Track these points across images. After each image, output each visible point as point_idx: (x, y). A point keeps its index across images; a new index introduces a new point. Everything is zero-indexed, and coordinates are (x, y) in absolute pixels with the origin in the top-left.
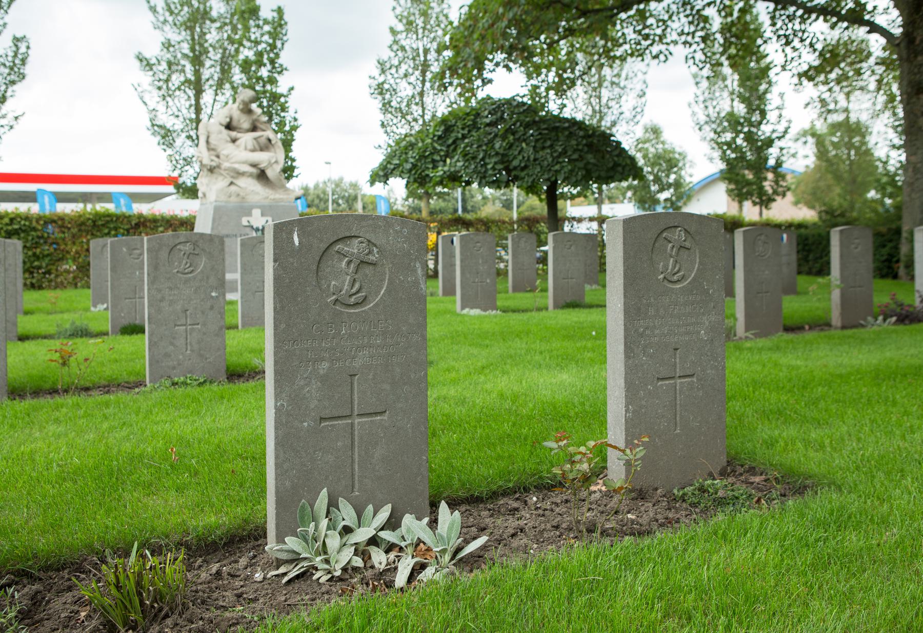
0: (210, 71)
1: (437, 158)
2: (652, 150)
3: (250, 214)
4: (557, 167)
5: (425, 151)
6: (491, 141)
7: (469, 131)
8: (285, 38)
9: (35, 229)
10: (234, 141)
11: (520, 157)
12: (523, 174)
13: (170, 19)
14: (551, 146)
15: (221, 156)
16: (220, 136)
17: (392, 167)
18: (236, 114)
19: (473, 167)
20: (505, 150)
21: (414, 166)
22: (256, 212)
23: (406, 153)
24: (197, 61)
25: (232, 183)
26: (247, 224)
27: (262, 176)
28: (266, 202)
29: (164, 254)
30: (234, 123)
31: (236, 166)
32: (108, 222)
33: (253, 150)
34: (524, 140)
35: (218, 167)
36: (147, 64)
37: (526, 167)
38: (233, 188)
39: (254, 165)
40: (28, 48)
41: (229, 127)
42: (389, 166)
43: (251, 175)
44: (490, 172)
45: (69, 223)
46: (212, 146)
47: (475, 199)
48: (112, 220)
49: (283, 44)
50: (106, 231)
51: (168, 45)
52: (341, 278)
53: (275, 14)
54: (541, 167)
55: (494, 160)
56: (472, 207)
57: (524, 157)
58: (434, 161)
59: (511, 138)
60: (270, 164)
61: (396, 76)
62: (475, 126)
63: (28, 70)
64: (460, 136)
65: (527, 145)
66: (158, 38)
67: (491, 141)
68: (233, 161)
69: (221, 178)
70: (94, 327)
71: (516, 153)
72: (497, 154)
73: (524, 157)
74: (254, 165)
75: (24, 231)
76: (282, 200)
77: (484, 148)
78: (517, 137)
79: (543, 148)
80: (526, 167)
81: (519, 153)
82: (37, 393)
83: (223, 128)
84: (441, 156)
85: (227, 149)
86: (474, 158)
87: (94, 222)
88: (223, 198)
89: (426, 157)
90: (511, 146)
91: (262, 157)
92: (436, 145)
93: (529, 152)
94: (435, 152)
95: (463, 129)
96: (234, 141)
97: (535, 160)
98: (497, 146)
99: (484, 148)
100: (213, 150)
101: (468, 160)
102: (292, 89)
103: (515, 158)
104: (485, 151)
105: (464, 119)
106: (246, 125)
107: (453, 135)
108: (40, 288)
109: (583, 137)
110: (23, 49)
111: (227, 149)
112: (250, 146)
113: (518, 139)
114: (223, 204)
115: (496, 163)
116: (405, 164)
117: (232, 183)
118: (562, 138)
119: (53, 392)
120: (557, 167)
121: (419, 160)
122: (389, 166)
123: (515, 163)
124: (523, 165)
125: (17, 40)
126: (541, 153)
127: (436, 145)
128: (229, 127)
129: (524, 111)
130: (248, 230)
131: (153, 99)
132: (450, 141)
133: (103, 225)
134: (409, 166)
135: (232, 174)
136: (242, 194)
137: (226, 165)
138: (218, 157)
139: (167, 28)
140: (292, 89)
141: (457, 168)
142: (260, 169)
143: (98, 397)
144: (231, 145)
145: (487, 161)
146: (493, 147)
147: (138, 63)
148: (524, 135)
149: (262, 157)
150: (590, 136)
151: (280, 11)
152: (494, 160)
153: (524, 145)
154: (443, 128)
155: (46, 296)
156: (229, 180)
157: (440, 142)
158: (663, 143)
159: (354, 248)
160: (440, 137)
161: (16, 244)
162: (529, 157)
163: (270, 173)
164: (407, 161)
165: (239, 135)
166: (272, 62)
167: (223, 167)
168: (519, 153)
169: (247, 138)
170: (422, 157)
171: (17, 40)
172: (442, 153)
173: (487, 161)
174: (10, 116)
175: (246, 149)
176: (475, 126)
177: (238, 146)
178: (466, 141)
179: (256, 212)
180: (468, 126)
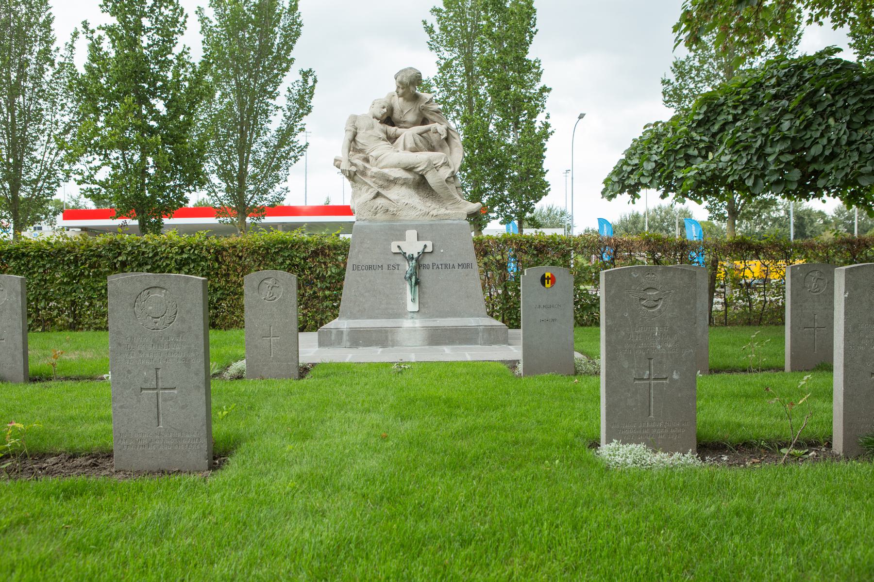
1: (693, 152)
3: (402, 238)
5: (676, 144)
7: (745, 110)
8: (533, 30)
9: (204, 259)
11: (825, 141)
12: (827, 168)
15: (371, 159)
16: (370, 132)
17: (629, 169)
19: (744, 161)
20: (798, 131)
21: (659, 165)
22: (411, 234)
23: (650, 149)
25: (378, 195)
26: (398, 251)
27: (421, 184)
28: (426, 220)
30: (397, 116)
31: (386, 171)
32: (281, 250)
33: (414, 150)
34: (833, 114)
35: (363, 173)
37: (833, 156)
38: (380, 201)
40: (315, 81)
42: (625, 168)
43: (405, 183)
44: (772, 167)
45: (241, 251)
46: (360, 147)
47: (815, 224)
48: (286, 248)
49: (531, 37)
50: (280, 260)
54: (860, 154)
55: (778, 148)
56: (812, 232)
57: (830, 140)
59: (810, 112)
61: (697, 79)
63: (314, 102)
64: (730, 118)
65: (836, 121)
67: (777, 121)
68: (381, 165)
69: (365, 188)
71: (818, 134)
72: (784, 138)
73: (830, 140)
74: (409, 169)
75: (194, 261)
76: (447, 217)
77: (764, 131)
78: (820, 109)
80: (833, 156)
81: (822, 136)
83: (377, 123)
84: (699, 150)
86: (746, 148)
87: (267, 249)
89: (676, 152)
90: (808, 126)
92: (694, 134)
93: (837, 129)
94: (691, 142)
95: (735, 107)
96: (392, 139)
97: (850, 143)
98: (786, 125)
99: (764, 131)
100: (361, 151)
101: (738, 151)
103: (815, 142)
104: (766, 136)
105: (738, 94)
106: (411, 117)
107: (721, 118)
110: (311, 83)
112: (410, 144)
113: (822, 114)
114: (366, 223)
115: (782, 153)
116: (645, 164)
117: (378, 195)
121: (667, 156)
122: (625, 168)
124: (827, 153)
125: (305, 74)
126: (861, 132)
127: (694, 134)
128: (389, 119)
129: (836, 71)
130: (399, 259)
132: (716, 127)
133: (277, 253)
135: (381, 183)
136: (391, 209)
137: (373, 169)
138: (367, 160)
141: (721, 165)
142: (417, 173)
145: (768, 150)
146: (778, 129)
148: (831, 105)
152: (778, 148)
153: (831, 121)
154: (705, 108)
156: (376, 189)
157: (701, 130)
160: (700, 123)
161: (14, 281)
162: (839, 139)
164: (648, 160)
165: (399, 130)
167: (369, 173)
168: (822, 136)
170: (671, 152)
171: (305, 74)
172: (702, 145)
173: (768, 150)
175: (405, 149)
176: (754, 101)
177: (396, 147)
178: (739, 124)
179: (411, 234)
180: (743, 103)
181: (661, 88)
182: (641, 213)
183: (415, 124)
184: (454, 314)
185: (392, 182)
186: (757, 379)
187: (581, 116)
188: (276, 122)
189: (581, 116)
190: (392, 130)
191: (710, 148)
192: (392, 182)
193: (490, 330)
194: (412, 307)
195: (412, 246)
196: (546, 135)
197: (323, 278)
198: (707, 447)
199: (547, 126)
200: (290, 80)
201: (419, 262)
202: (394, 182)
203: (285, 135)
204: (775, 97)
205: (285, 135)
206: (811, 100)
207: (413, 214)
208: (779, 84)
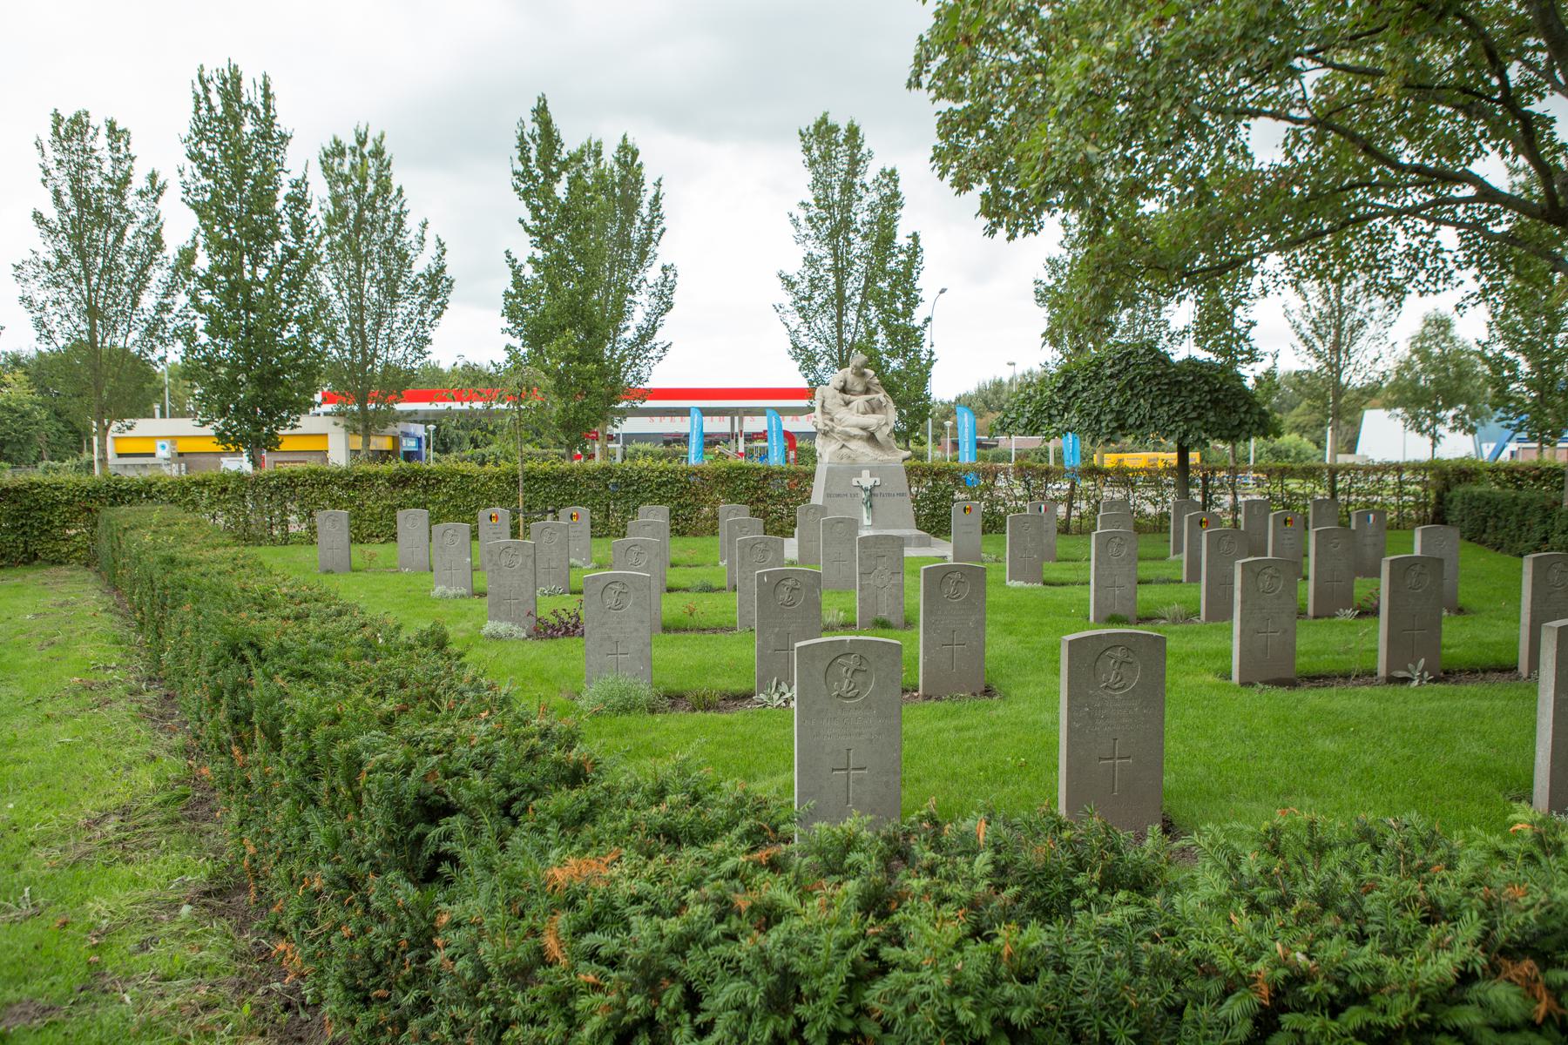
0: (854, 285)
2: (1436, 351)
4: (1172, 427)
6: (1108, 397)
9: (679, 481)
10: (847, 404)
13: (812, 233)
14: (1170, 403)
18: (850, 378)
22: (866, 473)
24: (840, 272)
27: (871, 438)
28: (875, 464)
29: (747, 550)
30: (849, 386)
33: (864, 414)
36: (789, 284)
37: (1141, 425)
38: (845, 450)
39: (863, 429)
41: (844, 390)
43: (861, 438)
51: (811, 261)
52: (784, 595)
53: (910, 241)
55: (1109, 417)
58: (1050, 416)
60: (879, 427)
62: (1097, 377)
63: (676, 298)
66: (800, 252)
67: (1108, 397)
70: (716, 585)
74: (863, 429)
76: (889, 461)
79: (1162, 405)
82: (677, 630)
85: (841, 413)
88: (836, 460)
91: (872, 420)
96: (847, 404)
98: (1114, 401)
102: (929, 319)
106: (859, 388)
108: (684, 534)
109: (1209, 392)
111: (841, 413)
118: (1184, 393)
119: (685, 630)
120: (1172, 427)
121: (1036, 414)
123: (1131, 421)
125: (664, 268)
128: (844, 390)
131: (795, 320)
134: (1024, 421)
139: (809, 243)
140: (929, 319)
143: (709, 635)
144: (844, 409)
147: (779, 281)
149: (872, 420)
150: (1216, 391)
151: (915, 237)
155: (690, 542)
158: (1452, 340)
159: (790, 583)
160: (1060, 389)
163: (878, 436)
166: (907, 294)
169: (859, 401)
174: (659, 347)
176: (1097, 377)
179: (866, 473)
181: (1033, 287)
182: (1006, 380)
183: (861, 393)
184: (895, 527)
185: (851, 437)
186: (1071, 564)
187: (943, 291)
188: (637, 318)
189: (943, 291)
190: (847, 397)
191: (1066, 409)
192: (851, 437)
193: (919, 537)
194: (867, 522)
195: (867, 480)
196: (931, 363)
197: (771, 497)
198: (1045, 583)
199: (932, 353)
200: (653, 274)
201: (871, 492)
202: (854, 437)
203: (646, 335)
204: (1111, 376)
205: (646, 335)
206: (1130, 385)
207: (866, 459)
208: (1114, 364)
